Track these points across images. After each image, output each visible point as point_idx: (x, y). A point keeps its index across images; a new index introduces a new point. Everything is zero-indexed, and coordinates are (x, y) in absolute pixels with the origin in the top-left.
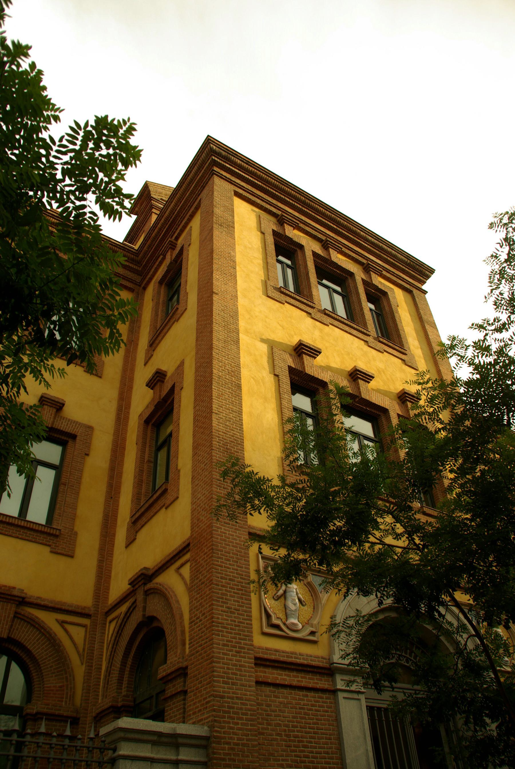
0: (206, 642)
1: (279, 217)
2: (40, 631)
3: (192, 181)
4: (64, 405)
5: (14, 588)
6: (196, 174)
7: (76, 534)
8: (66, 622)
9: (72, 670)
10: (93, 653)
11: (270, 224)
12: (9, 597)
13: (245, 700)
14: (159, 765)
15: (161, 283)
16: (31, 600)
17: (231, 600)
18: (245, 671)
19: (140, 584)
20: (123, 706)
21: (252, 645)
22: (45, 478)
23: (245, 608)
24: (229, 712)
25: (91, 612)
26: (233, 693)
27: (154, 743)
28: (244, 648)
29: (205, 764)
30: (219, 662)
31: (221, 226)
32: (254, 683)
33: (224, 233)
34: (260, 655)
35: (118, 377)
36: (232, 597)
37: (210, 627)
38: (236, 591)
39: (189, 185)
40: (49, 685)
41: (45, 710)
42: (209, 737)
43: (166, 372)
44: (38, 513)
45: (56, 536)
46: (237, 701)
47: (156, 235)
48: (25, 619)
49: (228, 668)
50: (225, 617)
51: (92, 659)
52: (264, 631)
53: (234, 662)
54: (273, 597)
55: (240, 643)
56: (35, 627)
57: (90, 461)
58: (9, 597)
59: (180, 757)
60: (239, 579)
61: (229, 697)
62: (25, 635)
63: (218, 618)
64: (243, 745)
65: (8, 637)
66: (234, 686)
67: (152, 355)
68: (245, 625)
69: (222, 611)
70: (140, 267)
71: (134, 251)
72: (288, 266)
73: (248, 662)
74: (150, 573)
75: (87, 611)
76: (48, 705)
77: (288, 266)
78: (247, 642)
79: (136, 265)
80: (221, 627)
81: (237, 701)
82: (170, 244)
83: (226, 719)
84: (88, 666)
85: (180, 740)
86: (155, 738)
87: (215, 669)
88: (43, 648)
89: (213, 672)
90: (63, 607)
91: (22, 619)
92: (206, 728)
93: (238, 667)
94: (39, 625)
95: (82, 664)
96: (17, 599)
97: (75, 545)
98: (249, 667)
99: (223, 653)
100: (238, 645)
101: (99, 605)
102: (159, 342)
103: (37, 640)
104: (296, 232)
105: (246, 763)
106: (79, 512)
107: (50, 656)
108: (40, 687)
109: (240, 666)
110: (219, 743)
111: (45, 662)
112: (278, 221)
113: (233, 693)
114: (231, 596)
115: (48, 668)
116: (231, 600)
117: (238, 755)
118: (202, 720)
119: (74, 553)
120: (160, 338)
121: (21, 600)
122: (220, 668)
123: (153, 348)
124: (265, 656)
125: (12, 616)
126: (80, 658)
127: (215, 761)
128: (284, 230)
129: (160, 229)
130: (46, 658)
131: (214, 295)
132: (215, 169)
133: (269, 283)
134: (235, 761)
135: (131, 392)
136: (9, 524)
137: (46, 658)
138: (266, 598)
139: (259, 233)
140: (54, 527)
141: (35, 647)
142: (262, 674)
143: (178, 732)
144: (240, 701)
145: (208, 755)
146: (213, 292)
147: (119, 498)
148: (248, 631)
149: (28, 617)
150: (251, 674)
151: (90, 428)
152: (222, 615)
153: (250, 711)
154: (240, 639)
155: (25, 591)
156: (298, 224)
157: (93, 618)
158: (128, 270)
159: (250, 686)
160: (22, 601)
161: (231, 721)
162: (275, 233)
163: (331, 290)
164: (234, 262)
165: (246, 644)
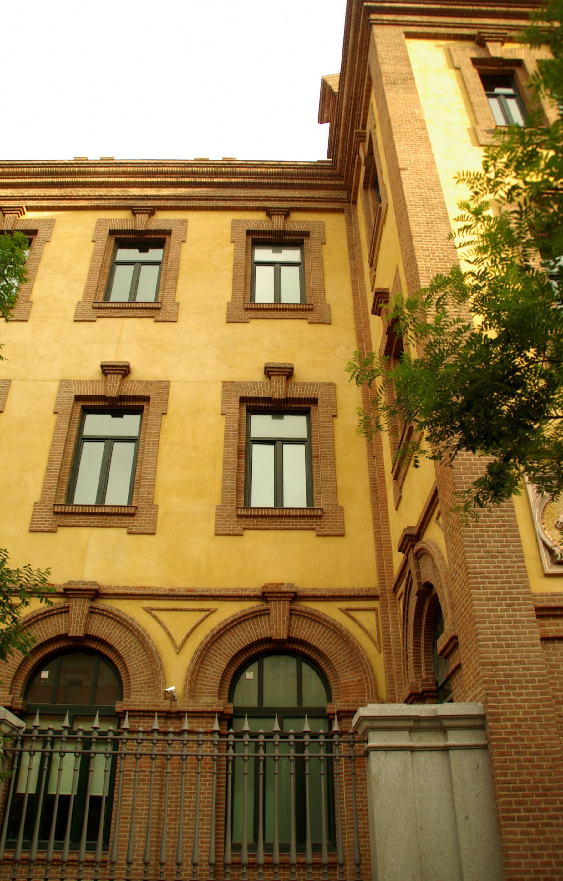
0: (467, 601)
1: (477, 38)
2: (324, 625)
3: (354, 46)
4: (292, 369)
5: (282, 584)
6: (355, 36)
7: (342, 509)
8: (352, 610)
9: (368, 660)
10: (389, 638)
11: (466, 52)
12: (280, 595)
13: (528, 664)
14: (424, 753)
15: (365, 188)
16: (306, 593)
17: (490, 542)
18: (523, 627)
19: (408, 547)
20: (423, 692)
21: (530, 593)
22: (295, 456)
23: (512, 548)
24: (506, 682)
25: (378, 593)
26: (509, 657)
27: (411, 730)
28: (518, 599)
29: (484, 747)
30: (484, 622)
31: (395, 83)
32: (540, 641)
33: (401, 90)
34: (545, 604)
35: (350, 316)
36: (492, 537)
37: (467, 581)
38: (495, 529)
39: (353, 54)
40: (345, 681)
41: (346, 708)
42: (485, 715)
43: (387, 289)
44: (295, 497)
45: (320, 517)
46: (517, 666)
47: (344, 134)
48: (303, 614)
49: (498, 628)
50: (484, 564)
51: (389, 645)
52: (546, 572)
53: (506, 618)
54: (556, 527)
55: (512, 593)
56: (316, 621)
57: (338, 422)
58: (280, 595)
59: (449, 743)
60: (499, 513)
61: (503, 664)
62: (307, 632)
63: (475, 568)
64: (532, 719)
65: (288, 637)
66: (510, 649)
67: (375, 276)
68: (516, 569)
69: (478, 558)
70: (342, 180)
71: (329, 164)
72: (508, 96)
73: (527, 615)
74: (415, 532)
75: (372, 593)
76: (348, 701)
77: (508, 96)
78: (522, 590)
79: (337, 180)
80: (481, 578)
81: (517, 666)
82: (358, 137)
83: (504, 691)
84: (386, 653)
85: (446, 723)
86: (411, 723)
87: (479, 631)
88: (330, 643)
89: (477, 635)
90: (344, 594)
91: (300, 616)
92: (480, 704)
93: (513, 624)
94: (321, 618)
95: (380, 652)
96: (288, 595)
97: (344, 522)
98: (528, 621)
99: (487, 609)
100: (508, 596)
101: (385, 583)
102: (377, 258)
103: (322, 635)
104: (508, 46)
105: (540, 742)
106: (340, 484)
107: (339, 650)
108: (337, 685)
109: (515, 622)
110: (498, 720)
111: (336, 657)
112: (477, 43)
113: (509, 657)
114: (489, 536)
115: (340, 663)
116: (490, 542)
117: (527, 733)
118: (476, 696)
119: (344, 531)
120: (376, 252)
121: (293, 595)
122: (487, 628)
123: (374, 267)
124: (553, 604)
125: (287, 614)
126: (375, 645)
127: (494, 743)
128: (488, 51)
129: (345, 124)
130: (336, 652)
131: (402, 172)
132: (373, 17)
133: (478, 128)
134: (523, 740)
135: (369, 328)
136: (263, 517)
137: (336, 652)
138: (545, 529)
139: (453, 72)
140: (315, 507)
141: (321, 643)
142: (553, 628)
143: (440, 713)
144: (520, 666)
145: (487, 737)
146: (399, 169)
147: (382, 454)
148: (521, 577)
149: (305, 612)
150: (532, 629)
151: (332, 386)
152: (480, 563)
153: (537, 676)
154: (510, 588)
155: (296, 585)
156: (506, 34)
157: (381, 599)
158: (330, 189)
159: (533, 646)
160: (295, 597)
161: (511, 692)
162: (475, 62)
163: (502, 98)
164: (422, 121)
165: (520, 593)
